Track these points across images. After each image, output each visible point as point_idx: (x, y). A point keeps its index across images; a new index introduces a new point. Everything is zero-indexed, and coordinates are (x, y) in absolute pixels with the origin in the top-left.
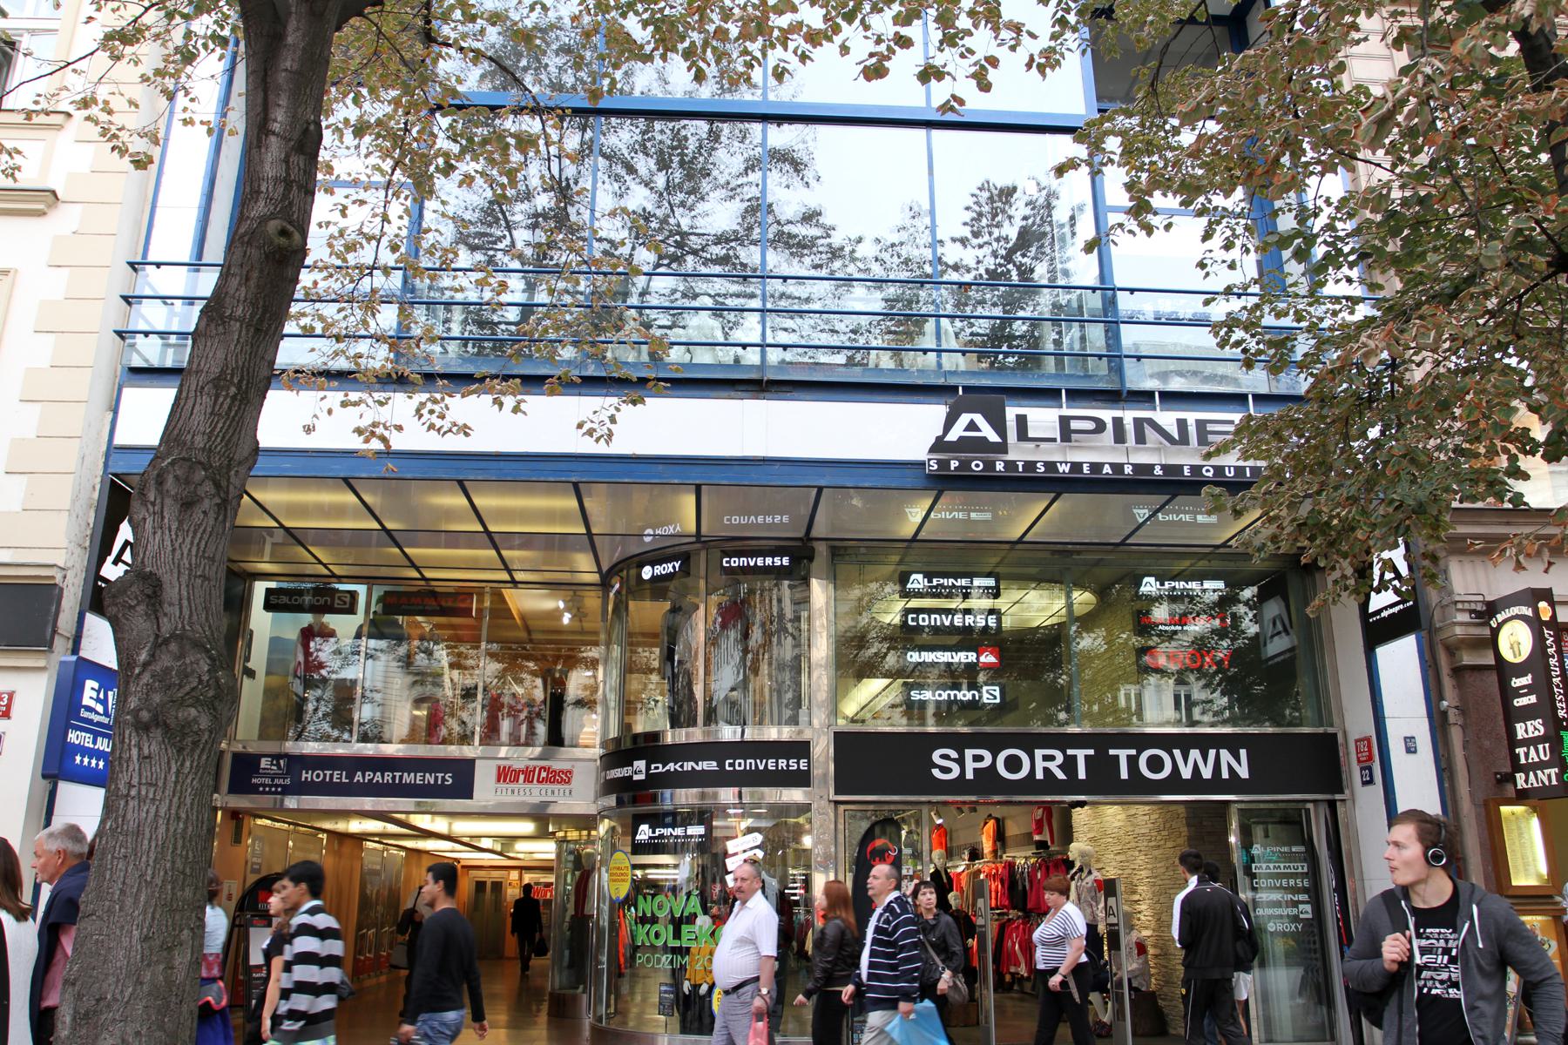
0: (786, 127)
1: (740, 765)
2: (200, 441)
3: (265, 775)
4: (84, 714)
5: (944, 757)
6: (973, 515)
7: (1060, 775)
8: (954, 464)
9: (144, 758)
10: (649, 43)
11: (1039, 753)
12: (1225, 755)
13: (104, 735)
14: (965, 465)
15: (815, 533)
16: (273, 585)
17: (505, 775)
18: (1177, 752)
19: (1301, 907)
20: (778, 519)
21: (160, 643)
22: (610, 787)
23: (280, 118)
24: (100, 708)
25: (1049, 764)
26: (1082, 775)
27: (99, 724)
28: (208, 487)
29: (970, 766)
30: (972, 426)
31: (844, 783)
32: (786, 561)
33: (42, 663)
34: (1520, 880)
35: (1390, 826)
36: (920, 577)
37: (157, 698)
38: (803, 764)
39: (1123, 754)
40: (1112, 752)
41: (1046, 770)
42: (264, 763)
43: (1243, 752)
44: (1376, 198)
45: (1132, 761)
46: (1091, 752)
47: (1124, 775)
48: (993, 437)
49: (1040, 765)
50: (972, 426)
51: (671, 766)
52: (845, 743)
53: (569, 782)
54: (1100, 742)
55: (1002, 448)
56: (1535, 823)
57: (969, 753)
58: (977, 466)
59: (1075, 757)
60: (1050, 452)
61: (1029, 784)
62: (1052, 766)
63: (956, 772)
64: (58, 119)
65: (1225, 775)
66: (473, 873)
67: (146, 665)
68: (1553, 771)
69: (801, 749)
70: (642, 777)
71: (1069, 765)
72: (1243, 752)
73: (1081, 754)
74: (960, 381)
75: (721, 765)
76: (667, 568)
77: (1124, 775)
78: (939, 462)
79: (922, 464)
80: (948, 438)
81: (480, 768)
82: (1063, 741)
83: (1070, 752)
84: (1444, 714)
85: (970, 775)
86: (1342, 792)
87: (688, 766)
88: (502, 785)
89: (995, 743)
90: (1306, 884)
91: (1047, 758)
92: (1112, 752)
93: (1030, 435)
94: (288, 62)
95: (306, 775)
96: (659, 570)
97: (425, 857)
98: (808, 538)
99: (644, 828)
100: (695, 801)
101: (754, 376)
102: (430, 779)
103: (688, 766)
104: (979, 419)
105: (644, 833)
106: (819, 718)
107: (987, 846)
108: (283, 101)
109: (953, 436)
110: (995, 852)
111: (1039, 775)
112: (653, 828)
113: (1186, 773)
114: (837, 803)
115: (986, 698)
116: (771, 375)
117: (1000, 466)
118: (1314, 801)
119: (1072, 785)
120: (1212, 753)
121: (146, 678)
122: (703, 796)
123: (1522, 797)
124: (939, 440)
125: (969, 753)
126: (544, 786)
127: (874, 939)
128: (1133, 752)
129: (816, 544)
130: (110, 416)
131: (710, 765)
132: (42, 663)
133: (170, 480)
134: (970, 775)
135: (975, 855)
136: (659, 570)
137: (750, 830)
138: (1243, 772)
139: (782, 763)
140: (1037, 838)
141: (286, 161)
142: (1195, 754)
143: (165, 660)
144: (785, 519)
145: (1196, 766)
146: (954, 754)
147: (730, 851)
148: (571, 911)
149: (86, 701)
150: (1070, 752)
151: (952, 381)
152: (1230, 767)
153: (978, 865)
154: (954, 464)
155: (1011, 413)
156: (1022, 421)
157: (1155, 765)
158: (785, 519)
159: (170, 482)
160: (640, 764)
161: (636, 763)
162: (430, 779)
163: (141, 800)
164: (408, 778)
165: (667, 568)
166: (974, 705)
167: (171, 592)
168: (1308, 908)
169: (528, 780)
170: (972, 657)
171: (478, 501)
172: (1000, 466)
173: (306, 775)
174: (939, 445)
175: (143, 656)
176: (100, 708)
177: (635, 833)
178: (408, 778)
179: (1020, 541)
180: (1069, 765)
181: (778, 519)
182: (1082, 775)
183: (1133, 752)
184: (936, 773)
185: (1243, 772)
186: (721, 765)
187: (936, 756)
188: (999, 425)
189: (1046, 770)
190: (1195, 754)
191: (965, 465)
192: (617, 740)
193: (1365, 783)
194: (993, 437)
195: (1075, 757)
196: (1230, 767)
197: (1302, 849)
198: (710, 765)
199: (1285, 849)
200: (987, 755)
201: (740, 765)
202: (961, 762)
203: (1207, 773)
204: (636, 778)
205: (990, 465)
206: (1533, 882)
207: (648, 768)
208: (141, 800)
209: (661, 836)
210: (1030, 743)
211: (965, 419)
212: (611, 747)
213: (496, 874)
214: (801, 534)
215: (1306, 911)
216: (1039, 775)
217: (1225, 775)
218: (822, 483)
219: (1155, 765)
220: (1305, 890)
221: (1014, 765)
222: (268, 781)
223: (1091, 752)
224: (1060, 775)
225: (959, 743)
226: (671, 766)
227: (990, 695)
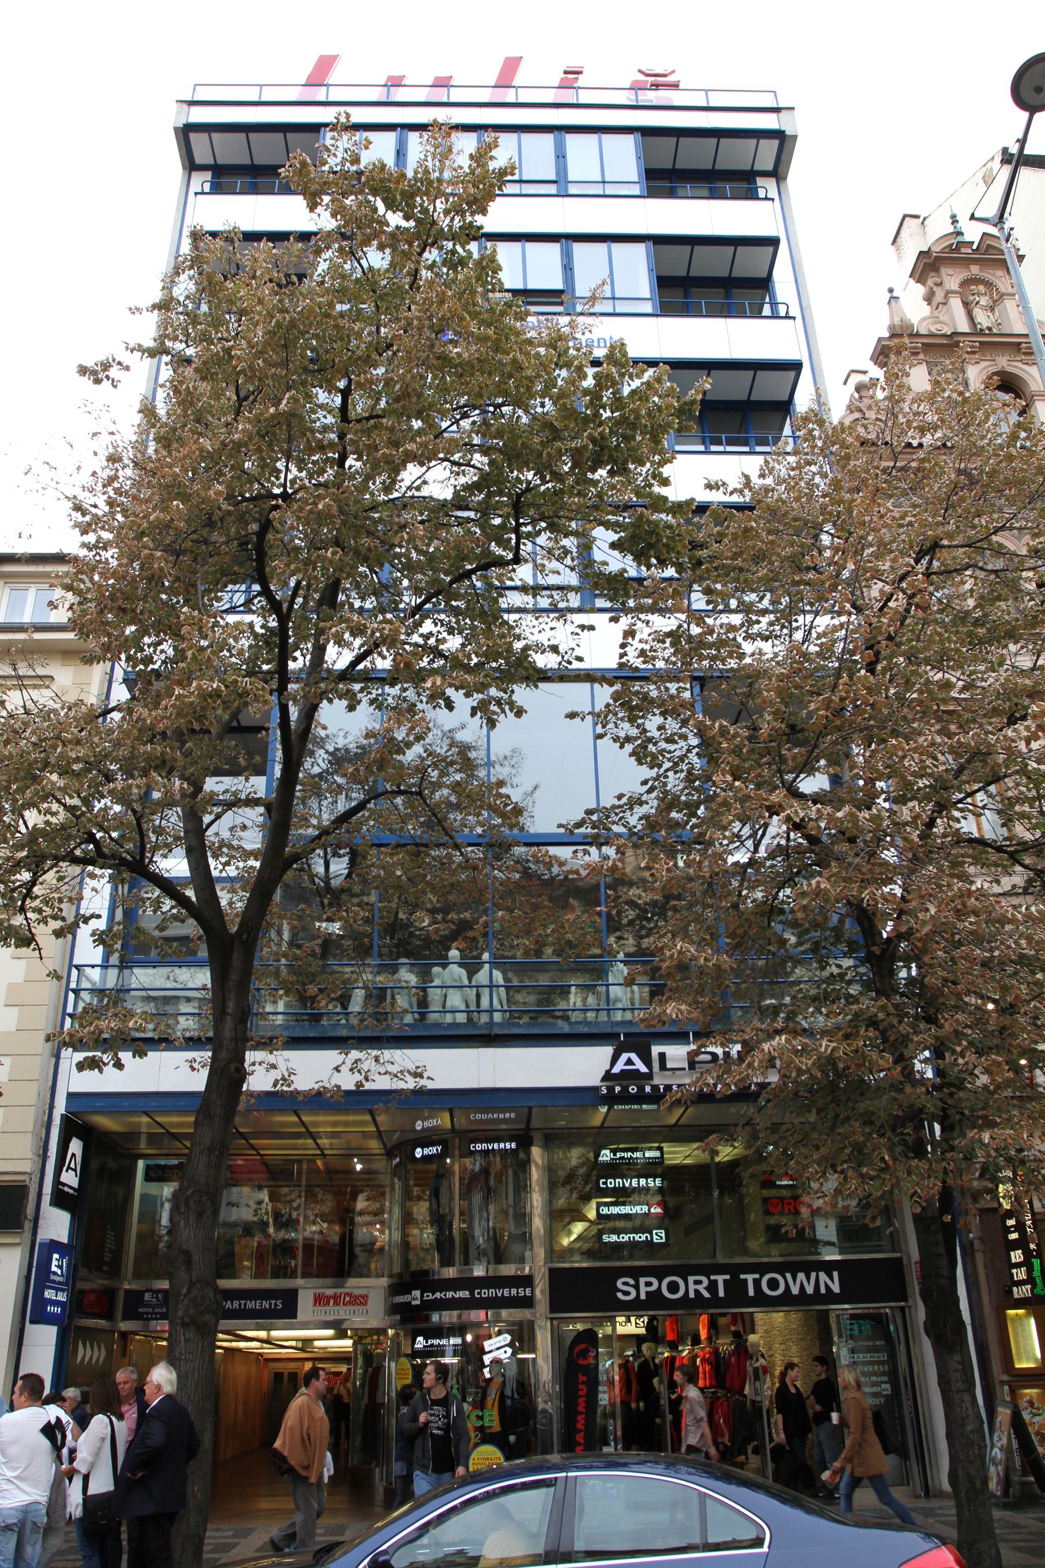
1: (486, 1293)
2: (203, 1180)
3: (148, 1306)
4: (53, 1277)
5: (625, 1284)
6: (644, 1107)
7: (706, 1295)
8: (618, 1089)
9: (187, 1340)
11: (691, 1279)
12: (823, 1276)
13: (63, 1290)
14: (625, 1089)
15: (534, 1124)
16: (151, 1162)
17: (319, 1300)
18: (788, 1276)
19: (883, 1386)
20: (507, 1115)
21: (191, 1285)
22: (394, 1309)
23: (231, 1006)
24: (59, 1272)
25: (698, 1287)
26: (721, 1294)
27: (59, 1283)
28: (209, 1204)
29: (643, 1290)
30: (629, 1062)
32: (514, 1145)
33: (18, 1240)
34: (1022, 1364)
36: (607, 1152)
37: (191, 1311)
39: (750, 1278)
40: (742, 1276)
41: (697, 1291)
42: (147, 1296)
43: (835, 1274)
45: (757, 1283)
46: (728, 1277)
48: (643, 1069)
49: (692, 1287)
50: (629, 1062)
51: (438, 1295)
52: (556, 1276)
53: (366, 1304)
54: (734, 1270)
55: (649, 1076)
56: (1032, 1321)
57: (642, 1281)
58: (633, 1089)
59: (716, 1281)
60: (679, 1077)
62: (701, 1288)
65: (823, 1291)
66: (272, 1365)
67: (186, 1295)
68: (1029, 1287)
69: (527, 1281)
70: (418, 1302)
71: (712, 1287)
72: (835, 1274)
73: (720, 1279)
74: (622, 1031)
75: (472, 1293)
76: (433, 1150)
78: (608, 1088)
79: (596, 1089)
80: (614, 1071)
81: (301, 1294)
82: (706, 1270)
83: (713, 1277)
84: (971, 1243)
85: (643, 1296)
86: (906, 1300)
87: (450, 1294)
88: (318, 1308)
89: (660, 1273)
90: (886, 1368)
92: (742, 1276)
93: (669, 1066)
94: (234, 976)
96: (427, 1151)
97: (237, 1354)
98: (528, 1129)
99: (420, 1339)
100: (455, 1320)
101: (485, 1032)
102: (266, 1304)
103: (450, 1294)
104: (633, 1056)
105: (420, 1342)
106: (540, 1252)
107: (703, 1334)
108: (232, 997)
109: (616, 1070)
110: (709, 1339)
111: (692, 1295)
112: (426, 1339)
114: (552, 1319)
115: (655, 1240)
116: (497, 1031)
117: (648, 1089)
118: (891, 1308)
120: (813, 1275)
121: (186, 1301)
122: (460, 1316)
123: (1019, 1304)
124: (608, 1072)
125: (642, 1281)
126: (348, 1308)
128: (757, 1276)
129: (533, 1133)
130: (53, 1060)
132: (18, 1240)
133: (192, 1201)
134: (643, 1296)
135: (696, 1341)
136: (427, 1151)
137: (499, 1333)
138: (836, 1288)
139: (514, 1292)
140: (733, 1328)
141: (235, 1029)
142: (801, 1276)
143: (195, 1292)
144: (513, 1115)
145: (802, 1287)
146: (632, 1282)
147: (487, 1349)
148: (366, 1401)
149: (54, 1269)
150: (713, 1277)
151: (616, 1030)
152: (826, 1285)
153: (697, 1350)
154: (618, 1089)
155: (656, 1050)
156: (662, 1056)
157: (773, 1284)
158: (513, 1115)
159: (192, 1203)
160: (417, 1293)
161: (414, 1292)
162: (266, 1304)
163: (187, 1360)
164: (251, 1305)
165: (433, 1150)
166: (649, 1243)
167: (196, 1258)
168: (888, 1386)
169: (336, 1304)
170: (645, 1208)
171: (304, 1118)
172: (648, 1089)
174: (608, 1076)
175: (184, 1291)
176: (59, 1272)
177: (414, 1342)
178: (251, 1305)
179: (676, 1125)
180: (712, 1287)
181: (507, 1115)
182: (721, 1294)
183: (757, 1276)
184: (620, 1295)
185: (836, 1288)
186: (472, 1293)
187: (619, 1284)
188: (647, 1060)
189: (697, 1291)
190: (801, 1276)
191: (625, 1089)
192: (400, 1275)
194: (643, 1069)
195: (716, 1281)
196: (826, 1285)
197: (883, 1343)
199: (871, 1343)
201: (486, 1293)
202: (637, 1287)
203: (810, 1290)
204: (414, 1303)
205: (641, 1089)
206: (1032, 1365)
207: (422, 1296)
208: (187, 1360)
209: (432, 1345)
210: (685, 1272)
211: (624, 1057)
212: (395, 1280)
213: (292, 1365)
214: (523, 1126)
215: (887, 1388)
216: (692, 1295)
217: (823, 1291)
218: (531, 1104)
219: (773, 1284)
220: (883, 1374)
221: (673, 1287)
222: (150, 1310)
223: (728, 1277)
224: (706, 1295)
225: (636, 1273)
226: (438, 1295)
227: (659, 1236)
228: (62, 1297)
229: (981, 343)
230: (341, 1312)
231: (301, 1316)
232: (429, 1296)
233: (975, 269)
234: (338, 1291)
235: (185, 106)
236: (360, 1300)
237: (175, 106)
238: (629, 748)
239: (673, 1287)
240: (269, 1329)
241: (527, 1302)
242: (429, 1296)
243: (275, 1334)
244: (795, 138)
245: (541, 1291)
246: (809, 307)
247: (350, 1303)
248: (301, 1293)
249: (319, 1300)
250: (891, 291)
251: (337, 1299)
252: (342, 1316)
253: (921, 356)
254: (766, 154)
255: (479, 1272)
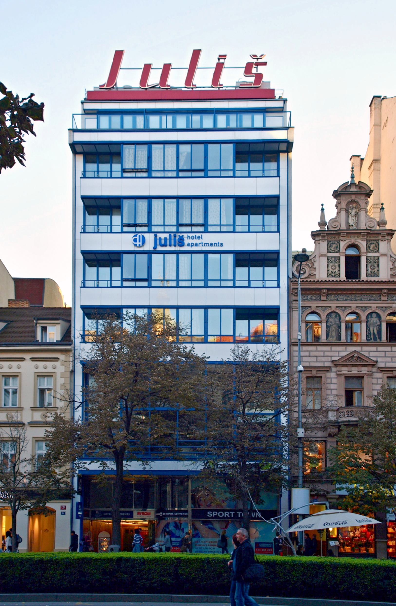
0: (180, 321)
1: (177, 514)
7: (229, 516)
10: (159, 331)
11: (225, 513)
17: (139, 513)
22: (157, 516)
26: (232, 516)
29: (214, 514)
31: (193, 517)
35: (373, 191)
38: (187, 514)
39: (239, 513)
42: (97, 512)
44: (379, 405)
45: (241, 514)
47: (239, 516)
49: (225, 515)
57: (214, 513)
61: (224, 517)
62: (227, 515)
63: (211, 516)
64: (56, 409)
65: (257, 517)
69: (186, 511)
71: (230, 515)
73: (232, 513)
77: (239, 516)
82: (229, 511)
87: (169, 514)
89: (218, 511)
91: (227, 513)
95: (104, 514)
102: (126, 514)
103: (169, 514)
113: (253, 516)
119: (230, 518)
125: (214, 513)
127: (82, 550)
131: (172, 514)
160: (161, 513)
162: (126, 514)
169: (143, 514)
173: (104, 514)
180: (230, 515)
182: (232, 516)
187: (208, 513)
193: (62, 512)
198: (172, 514)
200: (217, 513)
201: (177, 514)
202: (212, 514)
210: (224, 511)
216: (257, 517)
221: (221, 514)
224: (229, 516)
228: (81, 514)
229: (347, 233)
230: (144, 516)
231: (134, 517)
232: (164, 514)
233: (353, 197)
234: (143, 512)
235: (71, 132)
236: (149, 514)
237: (68, 131)
238: (314, 267)
239: (221, 514)
240: (126, 519)
241: (186, 516)
242: (164, 514)
243: (127, 520)
244: (292, 143)
245: (190, 514)
246: (291, 216)
247: (146, 514)
248: (134, 512)
249: (139, 513)
250: (322, 205)
251: (143, 513)
252: (144, 517)
253: (326, 238)
254: (283, 147)
255: (176, 509)
